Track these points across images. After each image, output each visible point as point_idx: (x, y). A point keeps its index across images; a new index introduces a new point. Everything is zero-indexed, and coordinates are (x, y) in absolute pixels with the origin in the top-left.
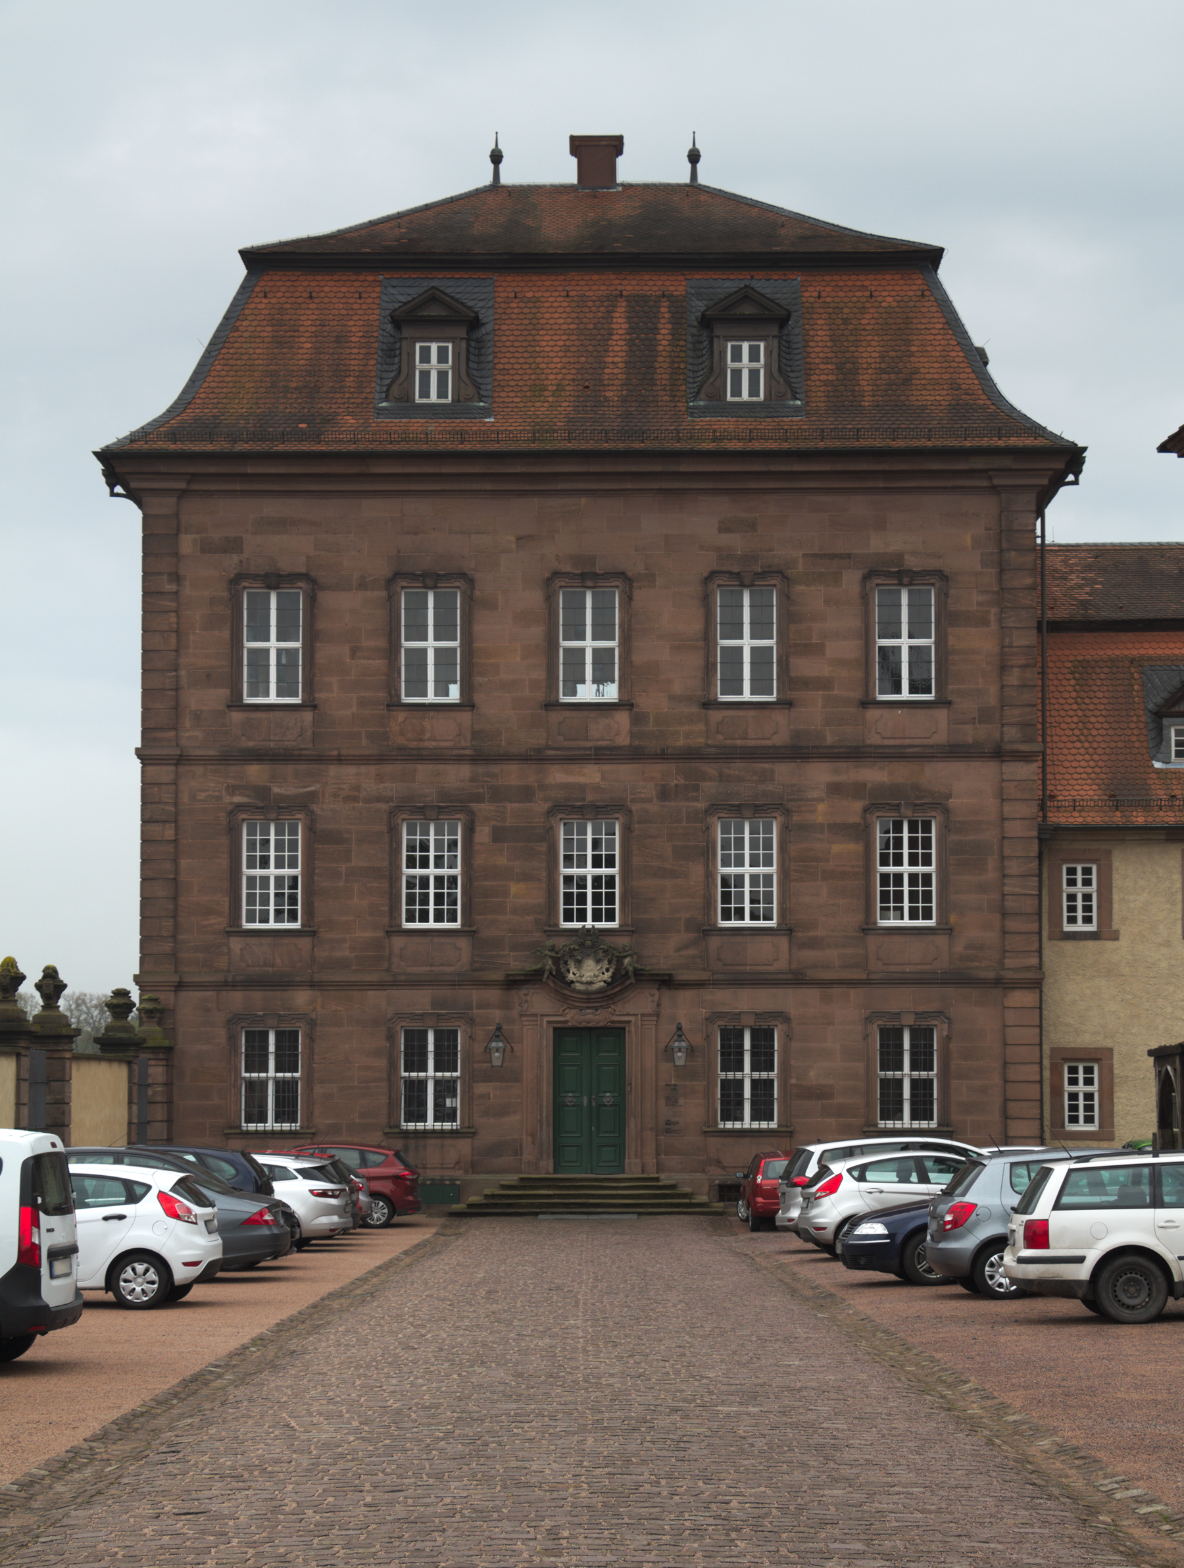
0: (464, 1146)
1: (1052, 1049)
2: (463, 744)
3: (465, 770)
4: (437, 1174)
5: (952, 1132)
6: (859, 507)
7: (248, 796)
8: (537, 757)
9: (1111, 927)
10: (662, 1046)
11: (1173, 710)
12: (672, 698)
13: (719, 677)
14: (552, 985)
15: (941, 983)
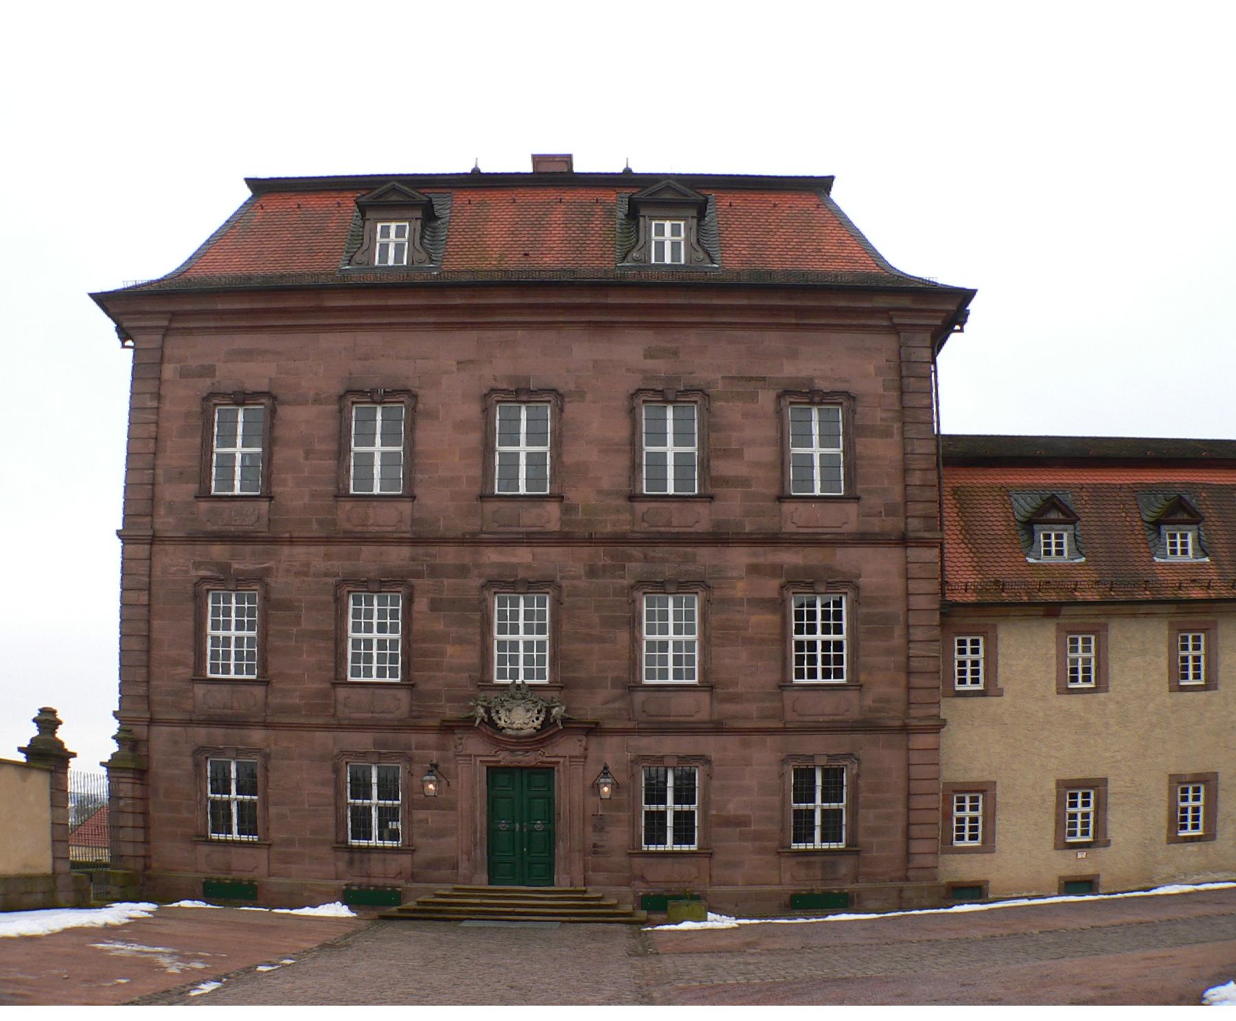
0: (405, 860)
1: (944, 783)
2: (404, 529)
3: (406, 551)
4: (381, 882)
5: (859, 851)
6: (773, 340)
7: (211, 571)
8: (473, 541)
9: (997, 685)
10: (589, 783)
11: (1044, 517)
12: (600, 492)
13: (644, 476)
14: (484, 730)
15: (851, 731)
